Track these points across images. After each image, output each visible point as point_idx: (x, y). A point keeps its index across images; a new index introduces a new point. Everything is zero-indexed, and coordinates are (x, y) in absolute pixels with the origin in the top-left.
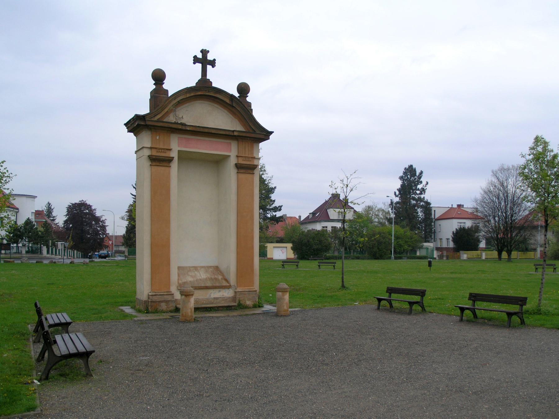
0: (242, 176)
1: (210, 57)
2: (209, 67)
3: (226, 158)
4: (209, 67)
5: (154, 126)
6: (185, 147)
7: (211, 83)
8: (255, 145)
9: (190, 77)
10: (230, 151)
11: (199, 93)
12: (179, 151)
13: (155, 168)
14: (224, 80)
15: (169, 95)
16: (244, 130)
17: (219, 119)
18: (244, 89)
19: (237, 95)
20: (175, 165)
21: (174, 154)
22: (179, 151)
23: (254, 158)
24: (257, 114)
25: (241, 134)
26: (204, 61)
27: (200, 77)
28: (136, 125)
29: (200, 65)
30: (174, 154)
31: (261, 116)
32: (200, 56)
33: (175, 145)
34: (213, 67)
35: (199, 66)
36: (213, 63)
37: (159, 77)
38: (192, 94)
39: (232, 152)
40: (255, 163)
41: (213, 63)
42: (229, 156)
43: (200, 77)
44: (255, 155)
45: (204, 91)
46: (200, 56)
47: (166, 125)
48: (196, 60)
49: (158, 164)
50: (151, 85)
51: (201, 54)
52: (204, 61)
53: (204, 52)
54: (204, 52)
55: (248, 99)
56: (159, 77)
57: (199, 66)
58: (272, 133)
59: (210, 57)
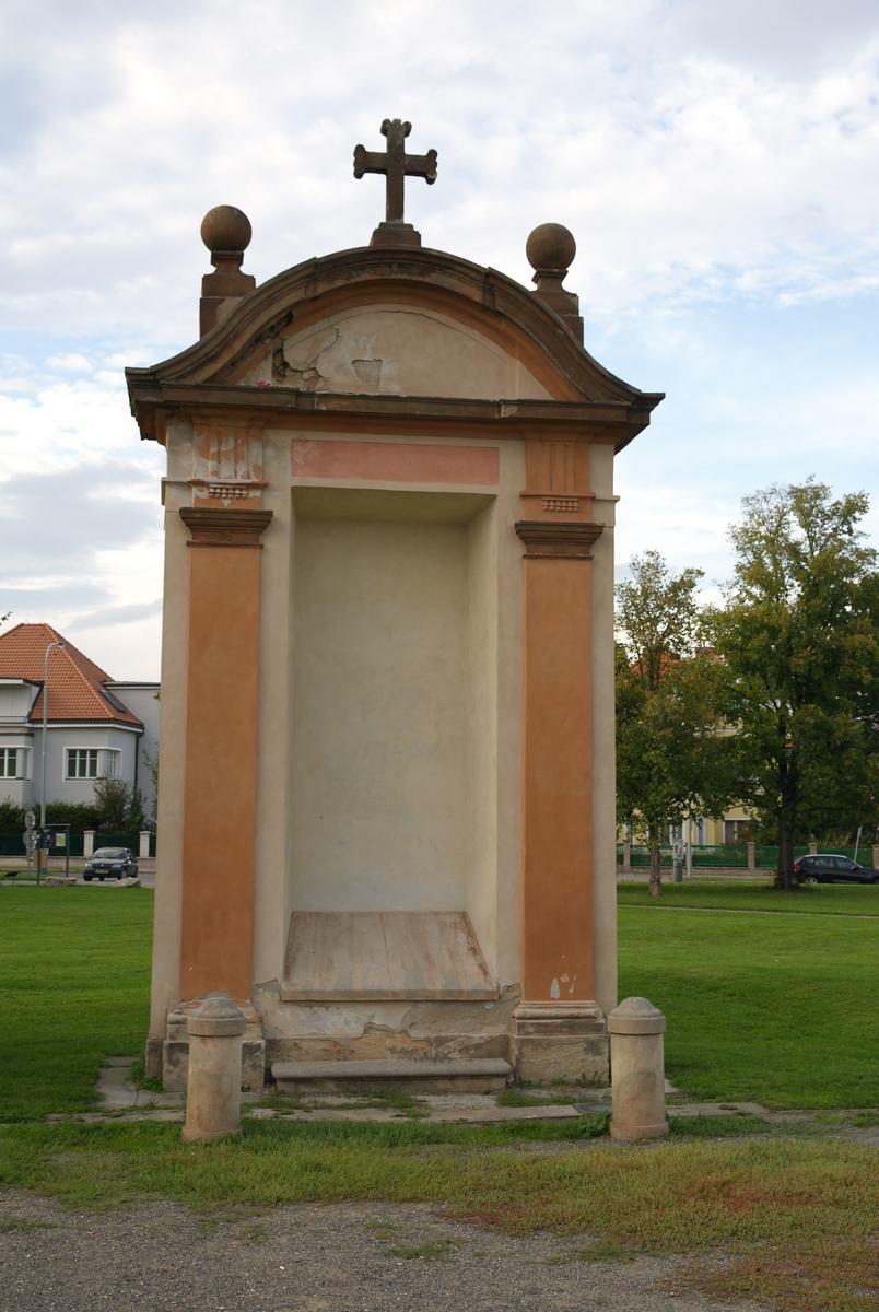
0: (549, 569)
1: (414, 147)
2: (413, 185)
3: (490, 499)
4: (413, 185)
5: (198, 406)
6: (321, 472)
7: (417, 236)
8: (596, 453)
9: (348, 218)
10: (493, 477)
11: (366, 276)
12: (295, 490)
13: (206, 554)
14: (473, 225)
15: (257, 286)
16: (548, 397)
17: (498, 375)
18: (552, 250)
19: (523, 274)
20: (278, 548)
21: (280, 505)
22: (295, 490)
23: (593, 499)
24: (597, 345)
25: (530, 413)
26: (395, 162)
27: (381, 216)
28: (159, 399)
29: (382, 178)
30: (280, 505)
31: (614, 342)
32: (378, 145)
33: (282, 470)
34: (360, 150)
35: (377, 182)
36: (426, 167)
37: (227, 235)
38: (340, 283)
39: (506, 480)
40: (597, 517)
41: (426, 167)
42: (490, 499)
43: (383, 219)
44: (600, 494)
45: (396, 269)
46: (378, 145)
47: (239, 398)
48: (364, 162)
49: (215, 541)
50: (202, 262)
51: (384, 139)
52: (395, 162)
53: (395, 131)
54: (395, 131)
55: (568, 284)
56: (227, 235)
57: (377, 182)
58: (656, 399)
59: (414, 147)
